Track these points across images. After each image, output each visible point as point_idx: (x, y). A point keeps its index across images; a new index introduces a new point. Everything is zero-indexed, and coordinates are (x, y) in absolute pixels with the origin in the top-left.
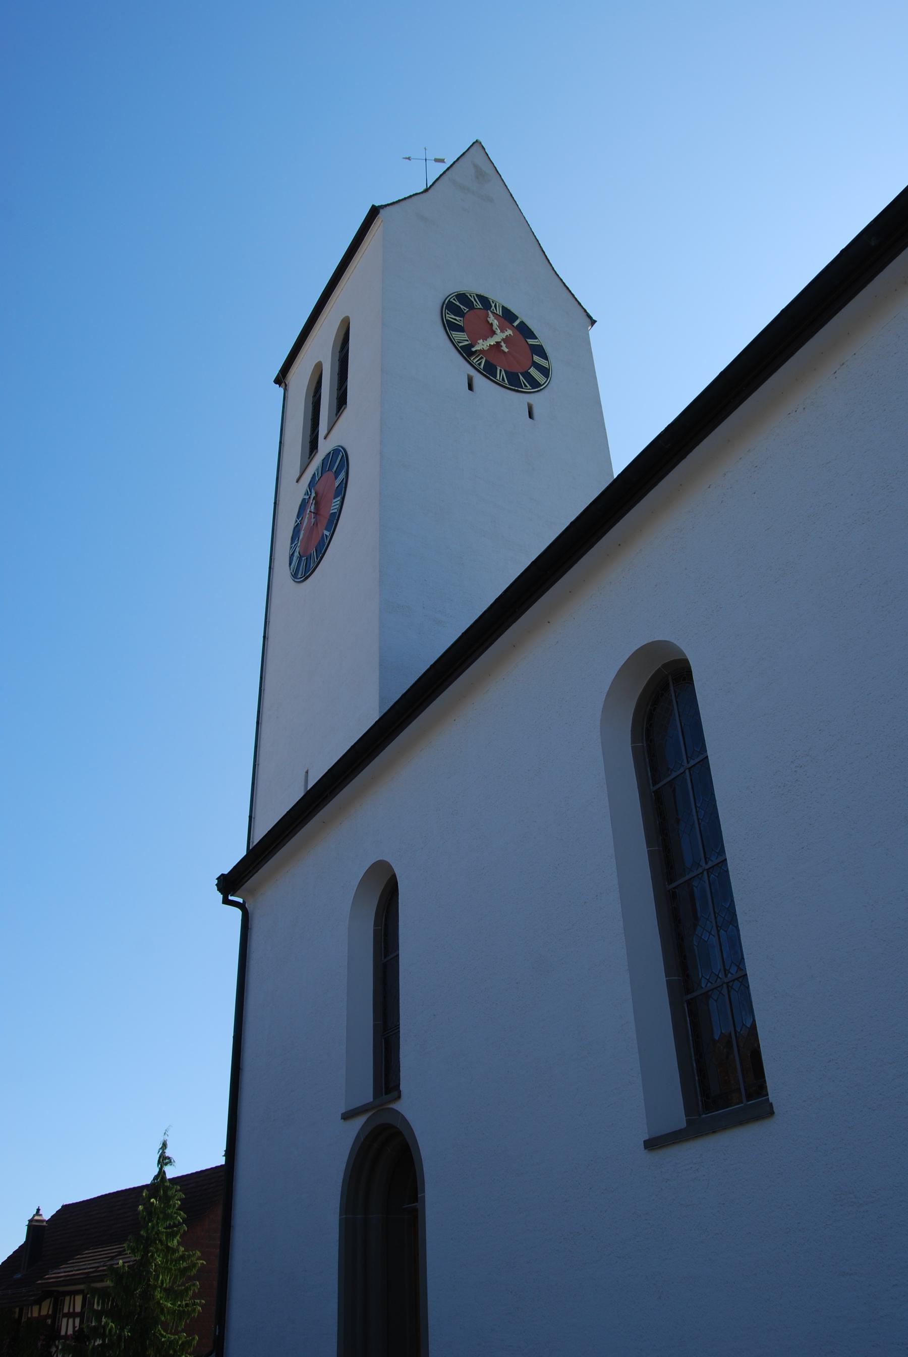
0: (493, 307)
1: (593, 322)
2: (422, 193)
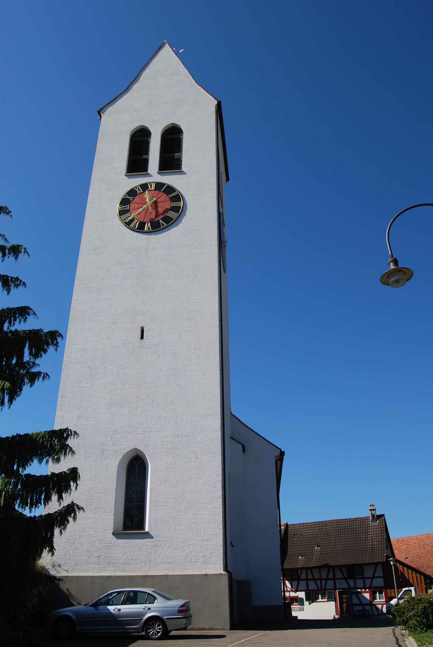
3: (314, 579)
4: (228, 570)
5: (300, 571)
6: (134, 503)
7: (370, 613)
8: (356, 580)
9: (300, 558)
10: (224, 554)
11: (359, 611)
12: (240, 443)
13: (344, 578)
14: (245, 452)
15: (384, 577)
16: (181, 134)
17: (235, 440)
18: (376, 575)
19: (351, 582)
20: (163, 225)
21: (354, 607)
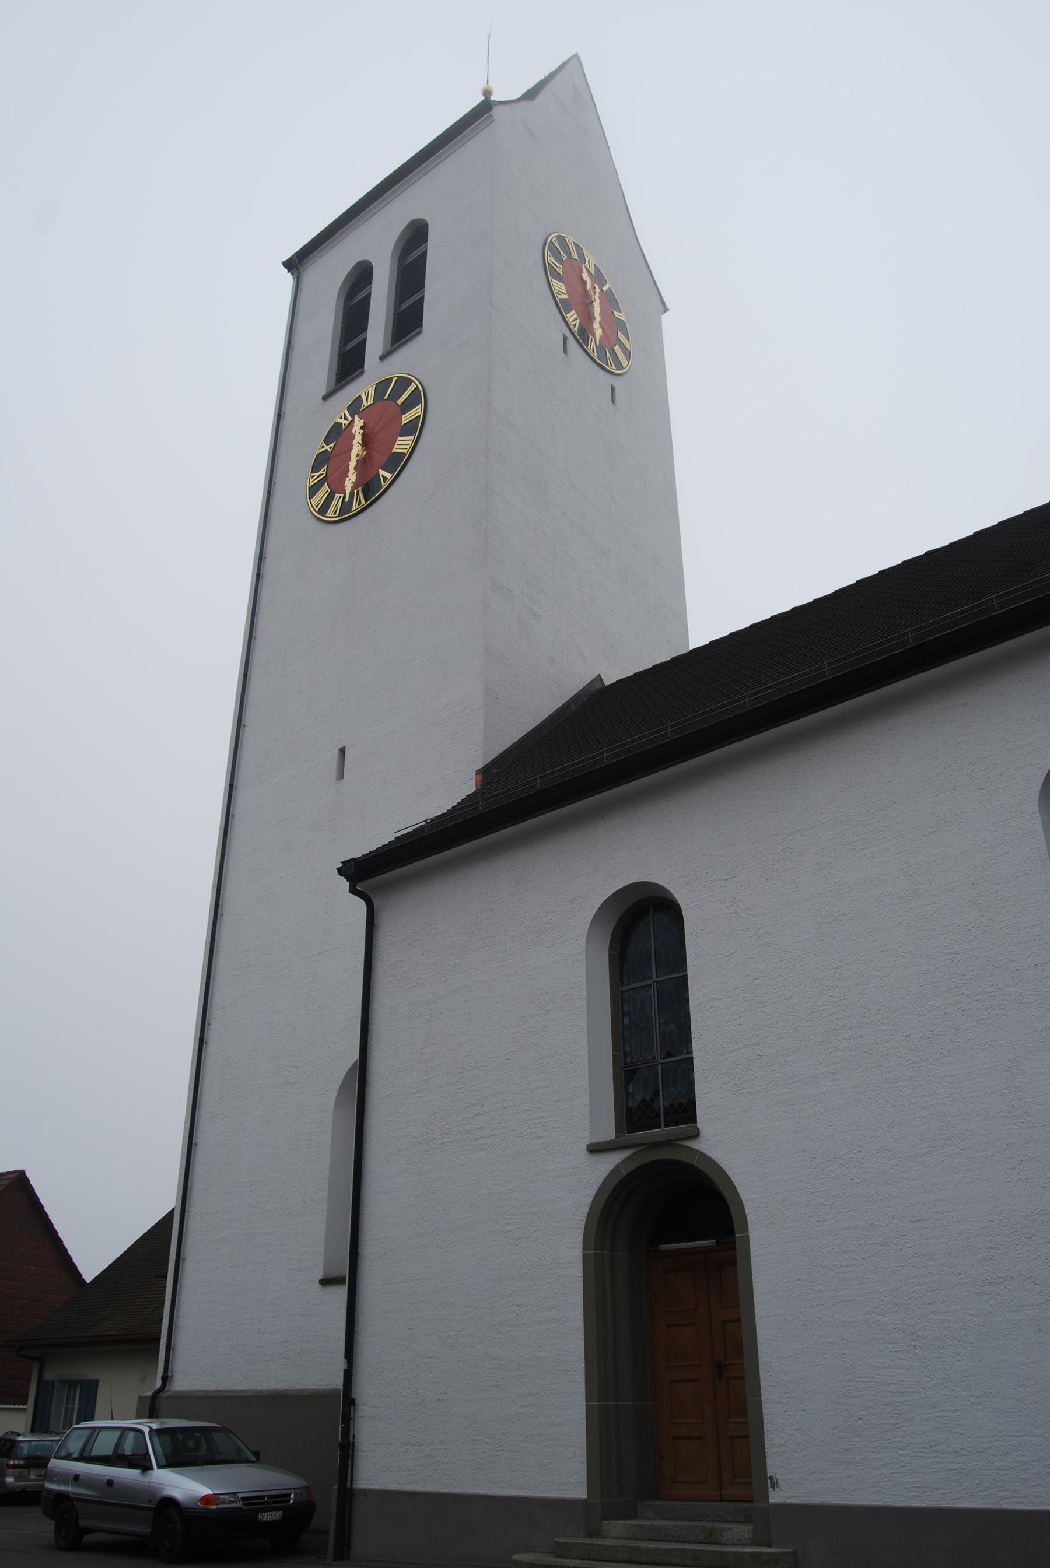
0: (587, 263)
1: (666, 310)
2: (519, 100)
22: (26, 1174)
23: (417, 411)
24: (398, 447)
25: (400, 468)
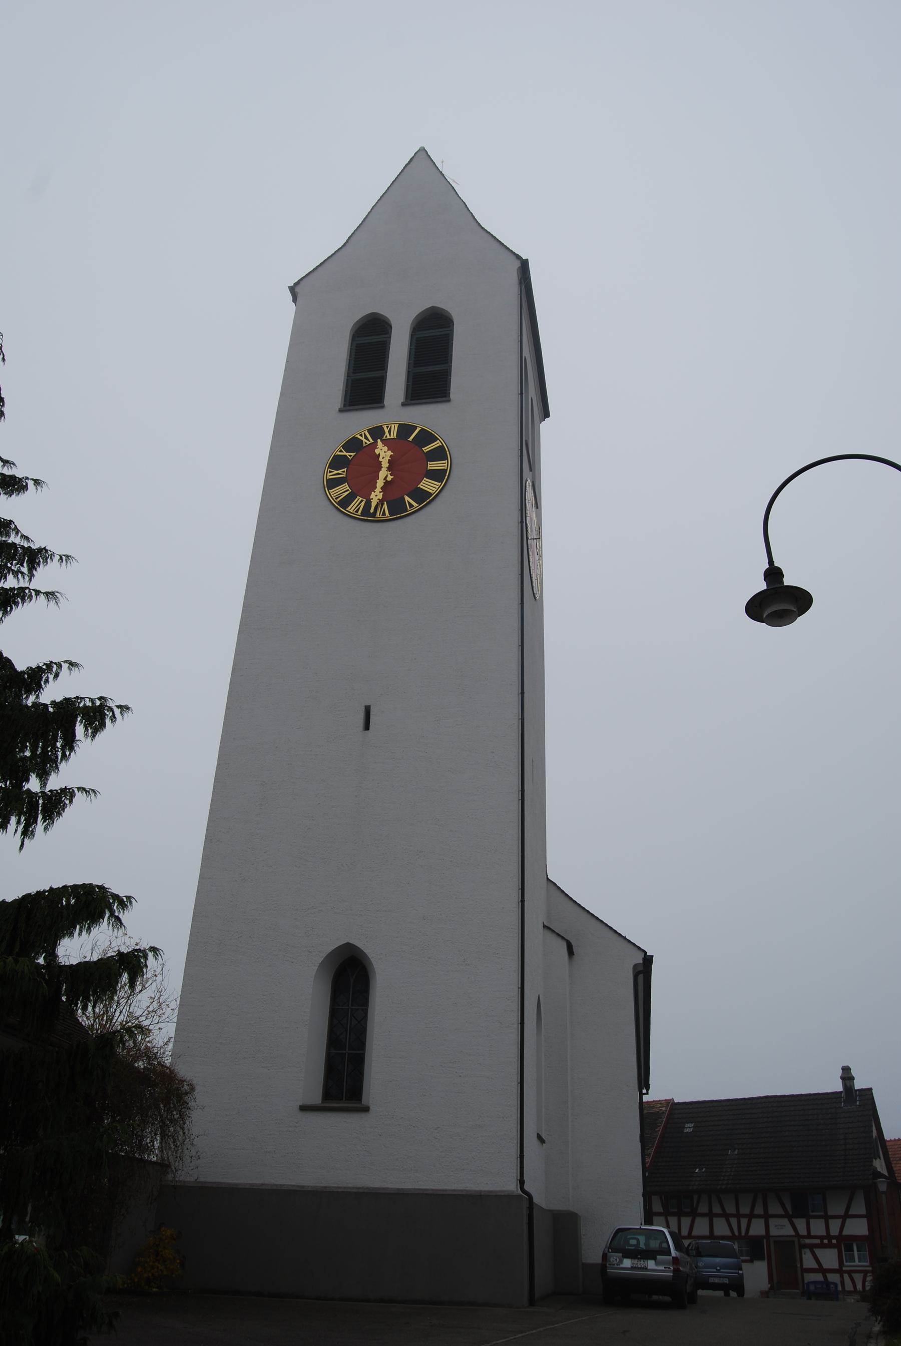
3: (726, 1216)
4: (524, 1189)
5: (695, 1197)
6: (345, 1050)
7: (840, 1288)
8: (812, 1221)
9: (697, 1171)
10: (519, 1156)
11: (815, 1283)
12: (563, 938)
13: (786, 1215)
14: (574, 954)
15: (869, 1216)
16: (449, 327)
17: (553, 931)
18: (852, 1212)
19: (801, 1224)
20: (411, 506)
21: (805, 1275)
22: (55, 887)
23: (333, 474)
24: (423, 484)
25: (426, 502)
